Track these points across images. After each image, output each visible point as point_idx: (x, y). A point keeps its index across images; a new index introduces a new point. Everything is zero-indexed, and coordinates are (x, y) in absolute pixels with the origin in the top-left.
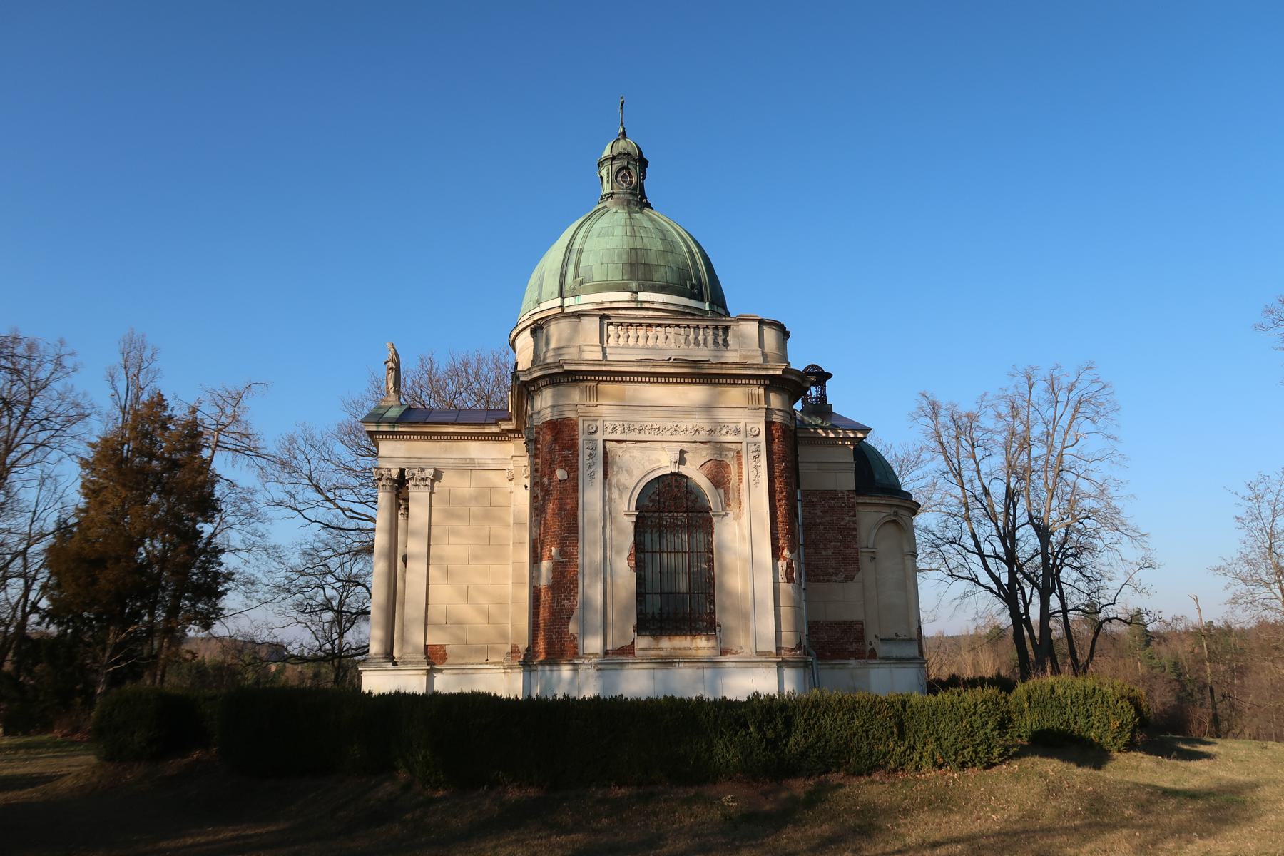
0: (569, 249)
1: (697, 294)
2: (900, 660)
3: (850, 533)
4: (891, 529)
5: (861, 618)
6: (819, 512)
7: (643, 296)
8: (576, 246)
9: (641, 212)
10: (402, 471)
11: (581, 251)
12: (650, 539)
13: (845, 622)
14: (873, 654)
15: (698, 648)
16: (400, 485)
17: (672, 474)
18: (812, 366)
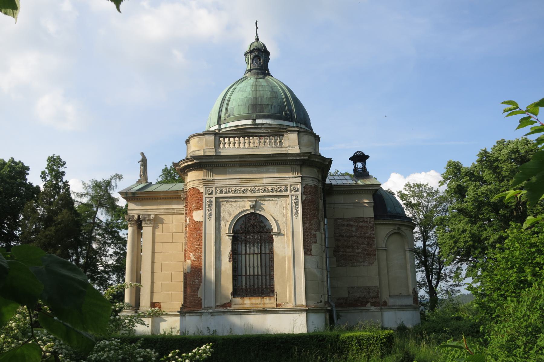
0: (223, 100)
1: (289, 118)
2: (402, 308)
3: (371, 240)
4: (395, 238)
5: (378, 284)
6: (354, 229)
7: (258, 121)
8: (227, 98)
9: (263, 78)
10: (139, 216)
11: (229, 100)
12: (242, 249)
13: (369, 288)
14: (385, 304)
15: (264, 304)
16: (139, 224)
17: (251, 213)
18: (359, 152)
